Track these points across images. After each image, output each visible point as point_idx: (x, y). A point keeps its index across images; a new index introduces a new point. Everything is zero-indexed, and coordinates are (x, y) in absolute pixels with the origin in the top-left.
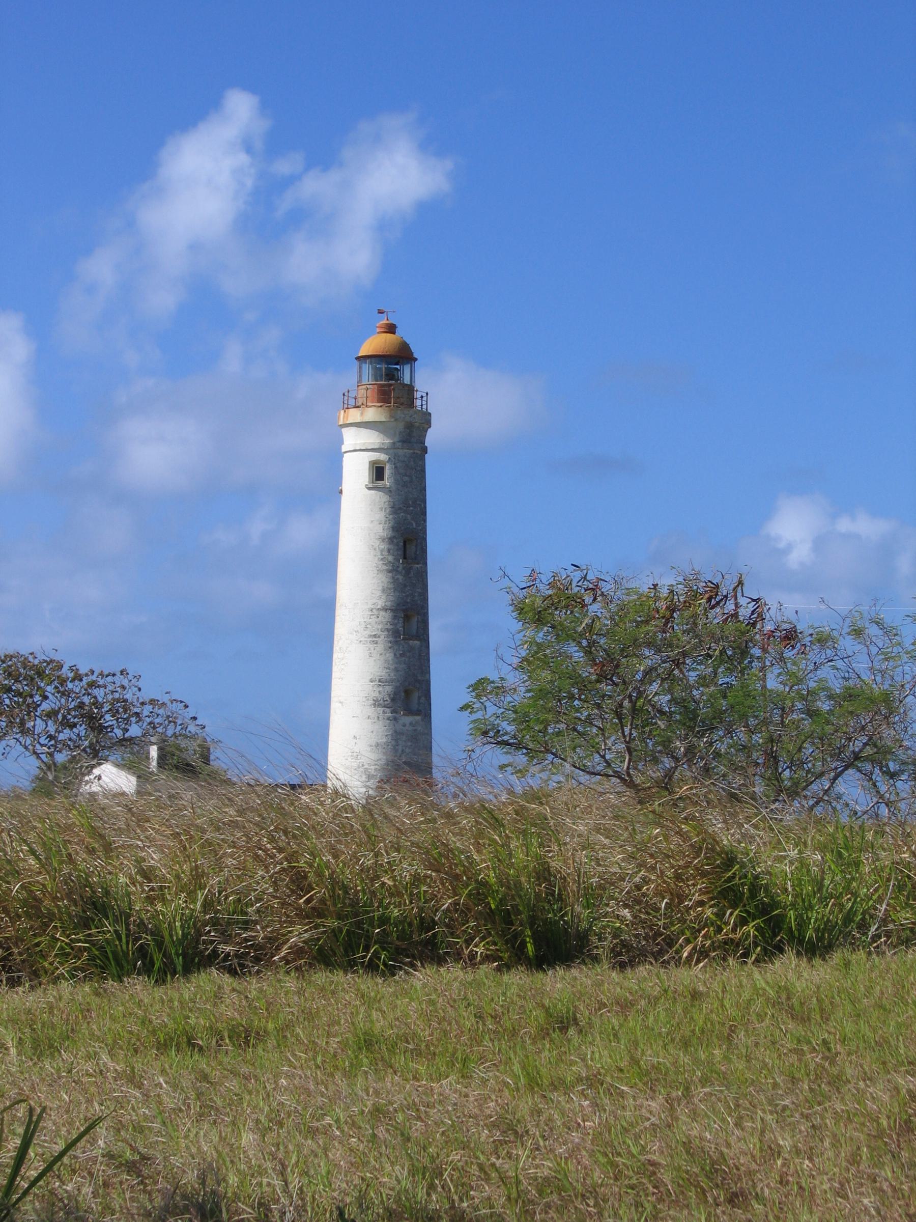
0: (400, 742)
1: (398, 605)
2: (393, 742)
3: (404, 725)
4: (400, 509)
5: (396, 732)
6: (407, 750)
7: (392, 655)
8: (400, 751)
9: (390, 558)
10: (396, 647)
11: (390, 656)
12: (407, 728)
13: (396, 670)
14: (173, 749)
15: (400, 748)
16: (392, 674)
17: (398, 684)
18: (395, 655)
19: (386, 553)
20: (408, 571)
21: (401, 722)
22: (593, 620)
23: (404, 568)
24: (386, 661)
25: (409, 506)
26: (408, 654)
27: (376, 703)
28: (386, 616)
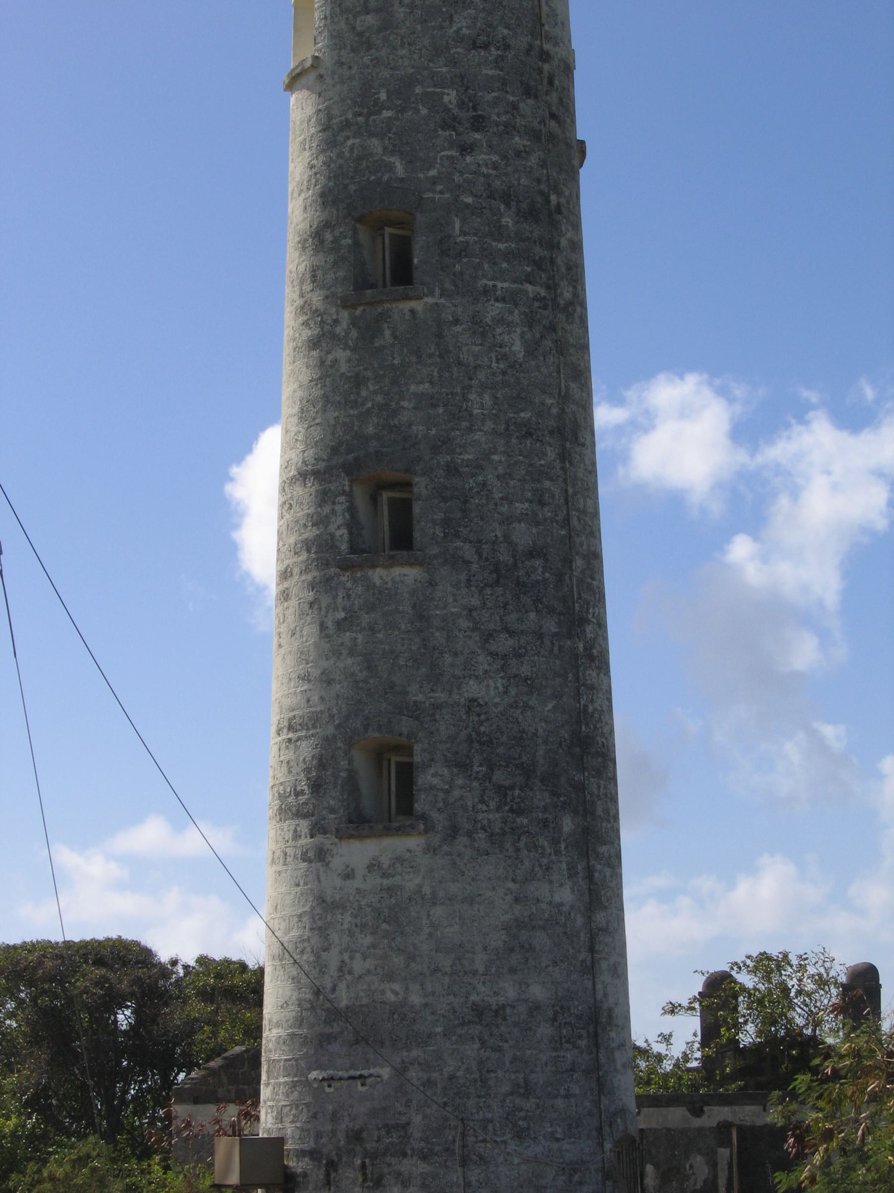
0: (334, 937)
1: (335, 450)
2: (315, 940)
3: (348, 875)
4: (347, 124)
5: (321, 900)
6: (358, 965)
7: (315, 628)
8: (334, 965)
9: (317, 299)
10: (325, 600)
11: (311, 631)
12: (357, 883)
13: (326, 679)
14: (576, 893)
15: (333, 958)
16: (315, 699)
17: (330, 730)
18: (323, 626)
19: (308, 287)
20: (368, 331)
21: (337, 863)
22: (178, 998)
23: (354, 322)
24: (302, 655)
25: (378, 107)
26: (366, 619)
27: (305, 678)
28: (304, 493)
